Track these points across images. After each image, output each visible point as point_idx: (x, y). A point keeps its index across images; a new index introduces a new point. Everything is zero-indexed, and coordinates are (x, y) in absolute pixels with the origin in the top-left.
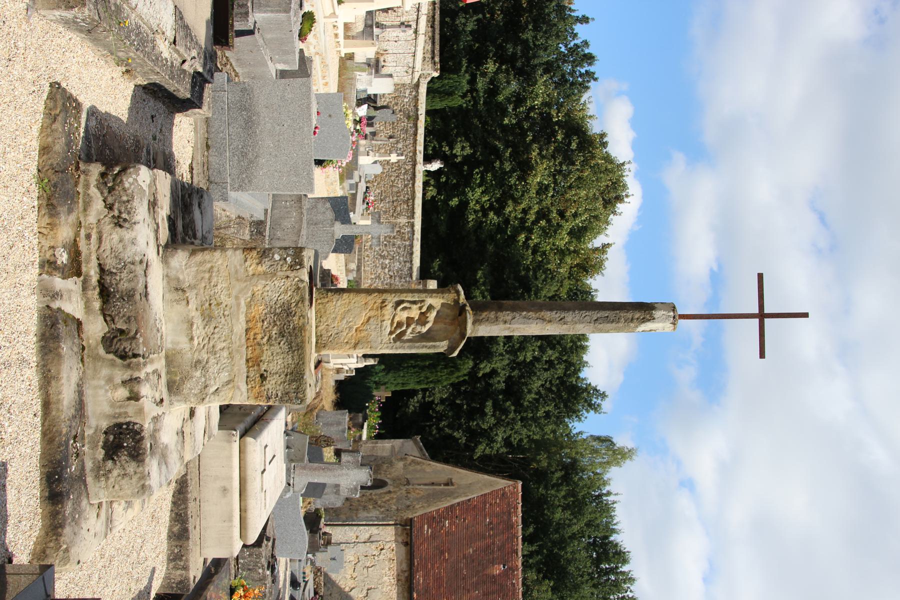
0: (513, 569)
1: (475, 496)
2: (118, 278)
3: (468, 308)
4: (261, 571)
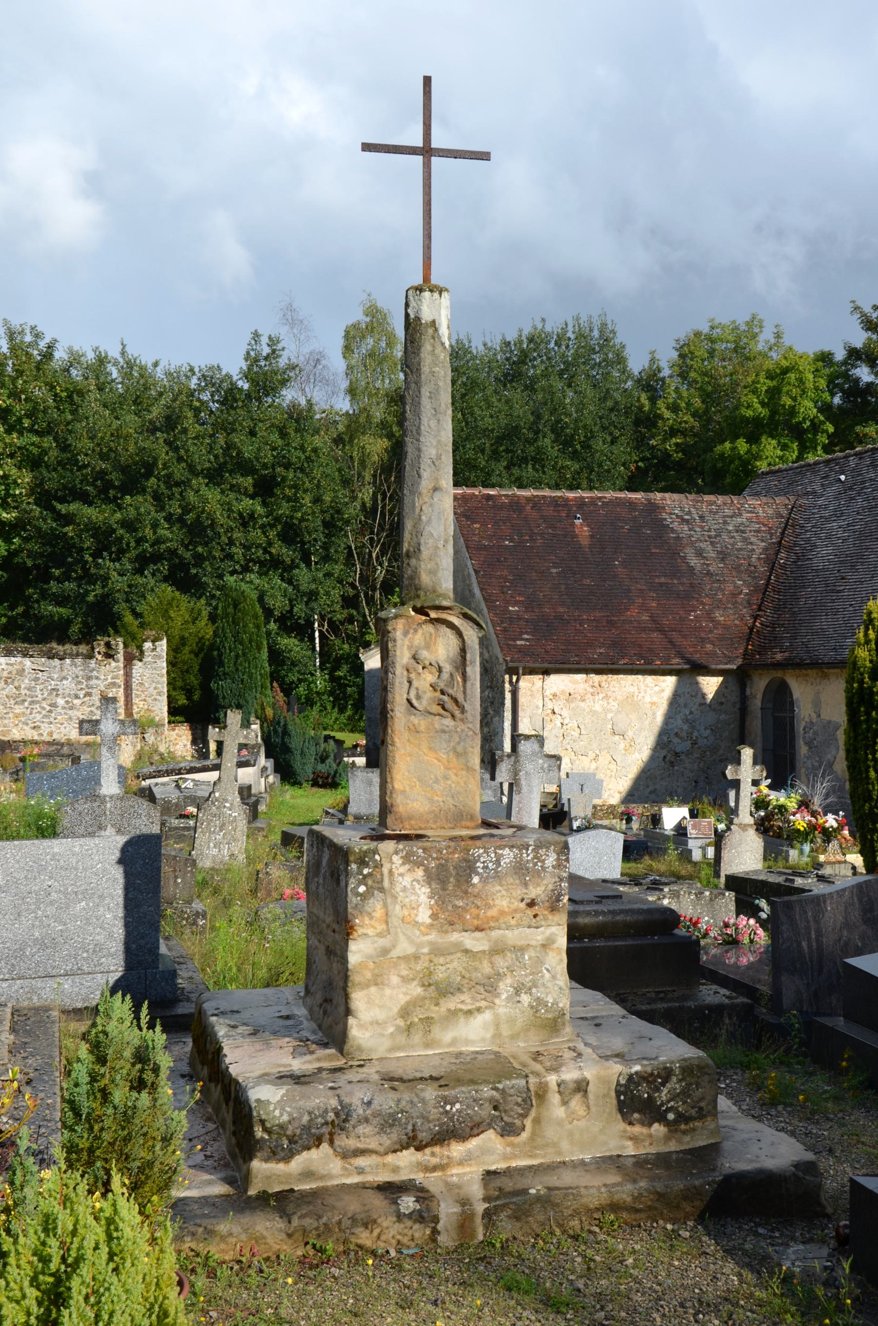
0: (581, 504)
1: (469, 563)
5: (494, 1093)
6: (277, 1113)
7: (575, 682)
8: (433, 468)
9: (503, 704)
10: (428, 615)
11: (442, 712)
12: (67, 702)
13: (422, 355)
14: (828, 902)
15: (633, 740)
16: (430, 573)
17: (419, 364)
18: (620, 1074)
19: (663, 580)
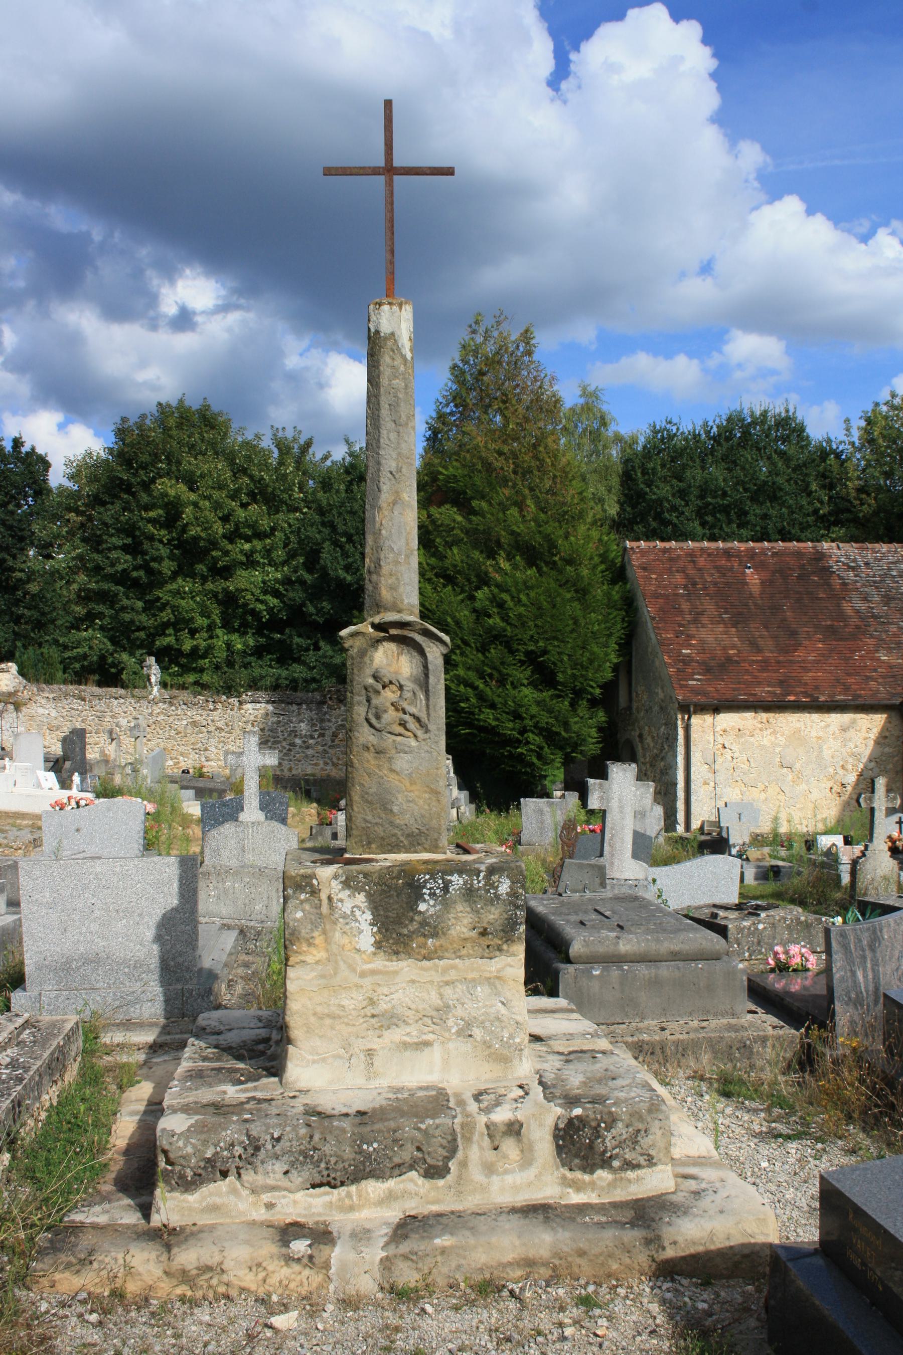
2: (333, 1160)
3: (377, 620)
4: (761, 926)
5: (417, 1133)
6: (181, 1143)
7: (746, 719)
8: (394, 481)
9: (676, 739)
12: (304, 742)
13: (381, 368)
14: (885, 930)
15: (800, 772)
16: (391, 588)
17: (379, 376)
18: (559, 1118)
19: (829, 623)
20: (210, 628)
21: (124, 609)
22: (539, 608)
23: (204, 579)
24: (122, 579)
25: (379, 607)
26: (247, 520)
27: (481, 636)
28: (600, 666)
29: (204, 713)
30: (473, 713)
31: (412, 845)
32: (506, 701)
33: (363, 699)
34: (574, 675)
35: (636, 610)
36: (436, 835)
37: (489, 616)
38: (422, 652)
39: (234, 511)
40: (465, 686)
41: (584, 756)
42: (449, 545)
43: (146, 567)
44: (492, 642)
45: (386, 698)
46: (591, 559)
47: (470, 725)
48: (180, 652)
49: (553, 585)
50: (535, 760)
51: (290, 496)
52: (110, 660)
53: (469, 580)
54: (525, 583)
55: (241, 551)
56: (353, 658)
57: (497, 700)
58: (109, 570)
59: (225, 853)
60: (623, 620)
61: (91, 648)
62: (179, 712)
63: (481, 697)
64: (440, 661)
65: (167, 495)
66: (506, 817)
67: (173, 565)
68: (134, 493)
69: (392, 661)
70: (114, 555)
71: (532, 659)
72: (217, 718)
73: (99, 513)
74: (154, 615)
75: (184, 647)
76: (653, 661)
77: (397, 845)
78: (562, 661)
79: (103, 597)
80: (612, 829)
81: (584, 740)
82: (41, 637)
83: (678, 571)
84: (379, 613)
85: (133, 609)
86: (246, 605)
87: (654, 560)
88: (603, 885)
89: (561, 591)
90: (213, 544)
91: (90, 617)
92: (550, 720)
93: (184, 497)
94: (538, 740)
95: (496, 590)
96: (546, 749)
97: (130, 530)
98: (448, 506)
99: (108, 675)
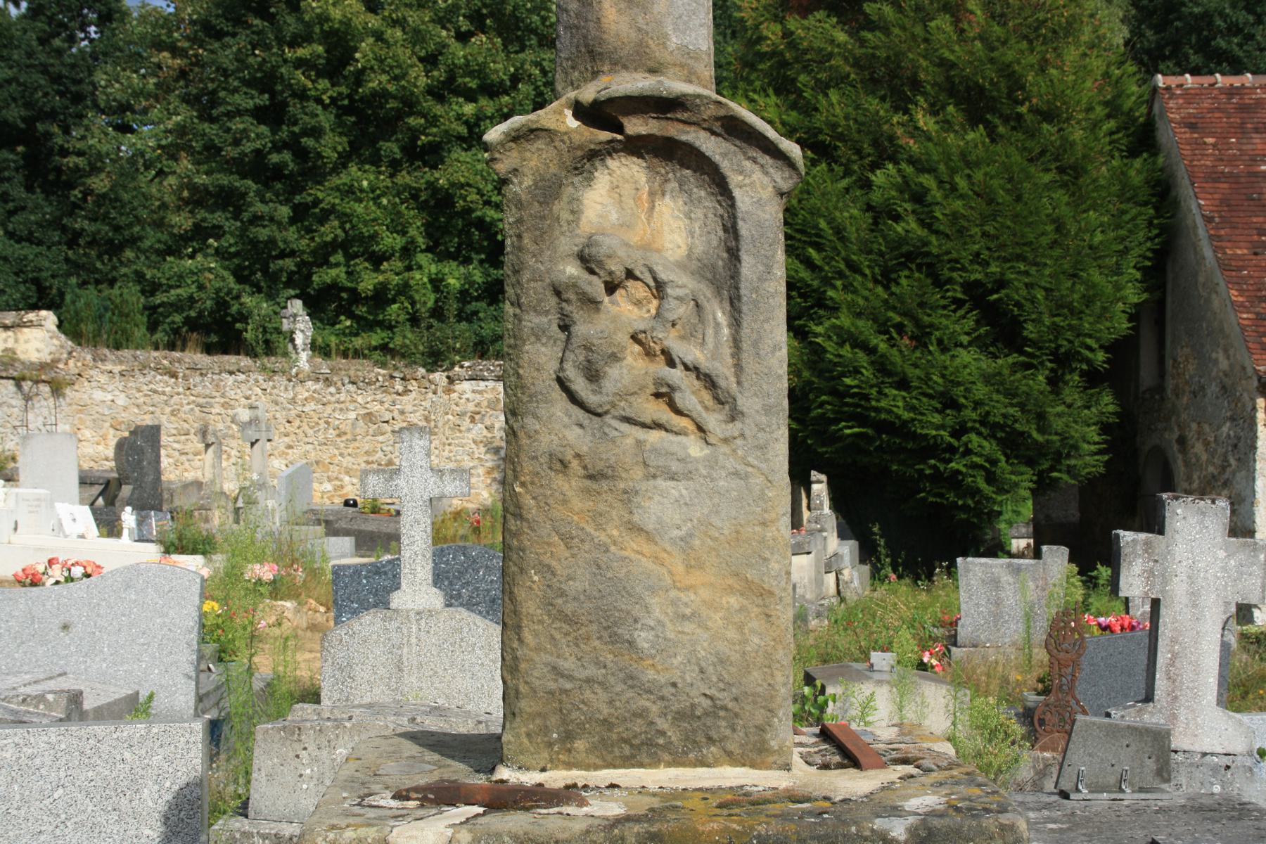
3: (588, 93)
10: (619, 129)
11: (665, 415)
20: (407, 251)
21: (256, 219)
22: (991, 201)
23: (395, 166)
24: (256, 167)
25: (595, 56)
26: (467, 64)
27: (881, 254)
28: (1105, 309)
29: (388, 399)
30: (866, 398)
31: (691, 741)
32: (928, 374)
33: (550, 322)
34: (1055, 329)
35: (1176, 204)
36: (759, 716)
37: (897, 218)
38: (720, 186)
39: (445, 46)
40: (853, 347)
41: (1074, 477)
42: (823, 87)
43: (293, 145)
44: (904, 266)
45: (615, 319)
46: (1090, 109)
47: (862, 420)
48: (355, 296)
49: (1017, 158)
50: (982, 484)
51: (544, 19)
52: (234, 309)
53: (859, 152)
54: (963, 155)
55: (459, 117)
56: (520, 205)
57: (912, 372)
58: (231, 152)
59: (363, 674)
60: (1150, 224)
61: (201, 287)
62: (342, 397)
63: (882, 367)
64: (773, 214)
65: (328, 19)
66: (929, 591)
67: (342, 143)
68: (273, 16)
69: (626, 209)
70: (237, 125)
71: (976, 295)
72: (409, 408)
73: (212, 52)
74: (309, 230)
75: (361, 287)
76: (1208, 301)
77: (649, 743)
78: (1033, 300)
79: (229, 200)
80: (1174, 641)
81: (1075, 447)
82: (114, 268)
83: (1257, 131)
84: (595, 74)
85: (272, 219)
86: (468, 211)
87: (1211, 111)
88: (1164, 772)
89: (1032, 170)
90: (409, 104)
91: (200, 233)
92: (1011, 411)
93: (357, 22)
94: (989, 447)
95: (909, 170)
96: (1003, 464)
97: (266, 81)
98: (820, 14)
99: (222, 333)
